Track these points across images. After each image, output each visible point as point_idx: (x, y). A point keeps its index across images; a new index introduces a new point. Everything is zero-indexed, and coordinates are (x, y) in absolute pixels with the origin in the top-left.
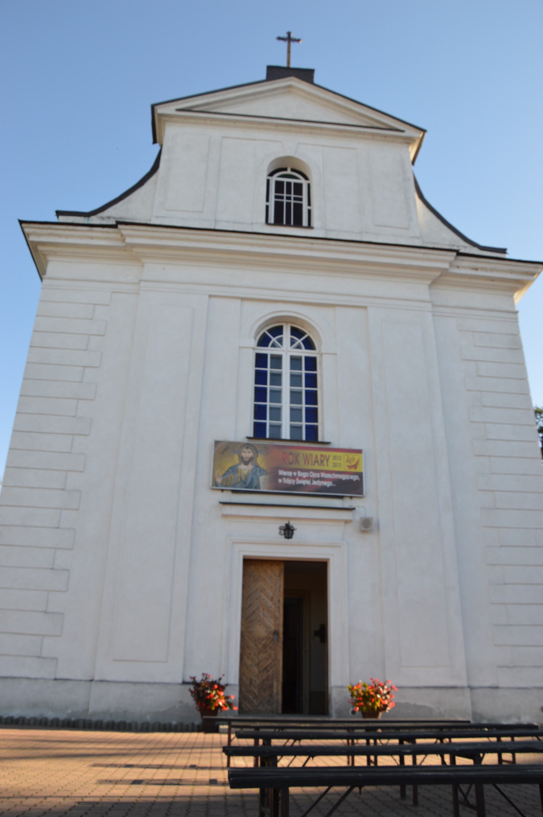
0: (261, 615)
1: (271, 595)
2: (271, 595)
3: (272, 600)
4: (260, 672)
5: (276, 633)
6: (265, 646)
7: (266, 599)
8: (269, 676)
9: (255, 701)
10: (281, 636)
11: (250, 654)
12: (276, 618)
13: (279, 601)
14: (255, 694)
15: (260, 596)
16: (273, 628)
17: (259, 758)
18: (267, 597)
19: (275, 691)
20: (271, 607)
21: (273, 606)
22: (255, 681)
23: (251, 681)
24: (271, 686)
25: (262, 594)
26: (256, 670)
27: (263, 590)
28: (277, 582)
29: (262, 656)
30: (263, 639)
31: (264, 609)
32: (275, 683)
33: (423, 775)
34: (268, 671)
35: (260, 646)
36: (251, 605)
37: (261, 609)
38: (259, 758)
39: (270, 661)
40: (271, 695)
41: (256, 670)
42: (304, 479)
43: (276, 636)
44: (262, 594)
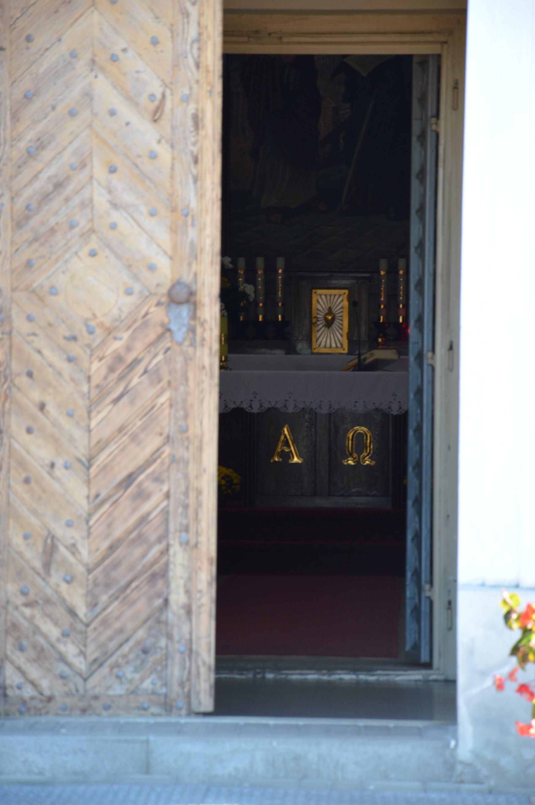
0: (101, 200)
1: (157, 89)
2: (157, 89)
3: (156, 116)
4: (97, 502)
5: (182, 296)
6: (122, 367)
7: (126, 112)
8: (143, 520)
9: (70, 650)
10: (211, 311)
11: (42, 407)
12: (181, 218)
13: (197, 121)
14: (72, 612)
15: (88, 95)
16: (166, 272)
17: (281, 262)
18: (131, 99)
19: (177, 598)
20: (153, 156)
21: (165, 153)
22: (73, 548)
23: (50, 550)
24: (159, 574)
25: (102, 86)
26: (76, 491)
27: (105, 62)
28: (186, 15)
29: (108, 418)
30: (110, 332)
31: (113, 170)
32: (178, 557)
33: (226, 678)
34: (142, 495)
35: (97, 368)
36: (41, 145)
37: (98, 169)
38: (281, 262)
39: (152, 443)
40: (158, 619)
41: (76, 491)
42: (197, 497)
43: (185, 311)
44: (102, 86)
